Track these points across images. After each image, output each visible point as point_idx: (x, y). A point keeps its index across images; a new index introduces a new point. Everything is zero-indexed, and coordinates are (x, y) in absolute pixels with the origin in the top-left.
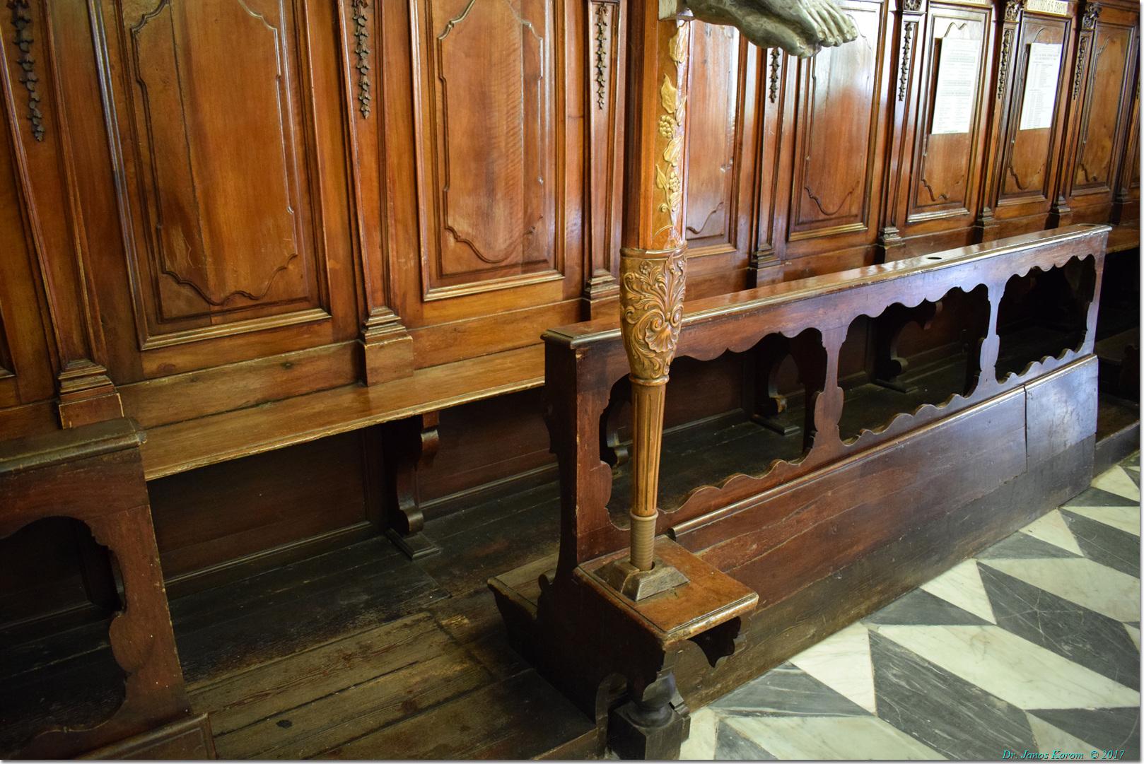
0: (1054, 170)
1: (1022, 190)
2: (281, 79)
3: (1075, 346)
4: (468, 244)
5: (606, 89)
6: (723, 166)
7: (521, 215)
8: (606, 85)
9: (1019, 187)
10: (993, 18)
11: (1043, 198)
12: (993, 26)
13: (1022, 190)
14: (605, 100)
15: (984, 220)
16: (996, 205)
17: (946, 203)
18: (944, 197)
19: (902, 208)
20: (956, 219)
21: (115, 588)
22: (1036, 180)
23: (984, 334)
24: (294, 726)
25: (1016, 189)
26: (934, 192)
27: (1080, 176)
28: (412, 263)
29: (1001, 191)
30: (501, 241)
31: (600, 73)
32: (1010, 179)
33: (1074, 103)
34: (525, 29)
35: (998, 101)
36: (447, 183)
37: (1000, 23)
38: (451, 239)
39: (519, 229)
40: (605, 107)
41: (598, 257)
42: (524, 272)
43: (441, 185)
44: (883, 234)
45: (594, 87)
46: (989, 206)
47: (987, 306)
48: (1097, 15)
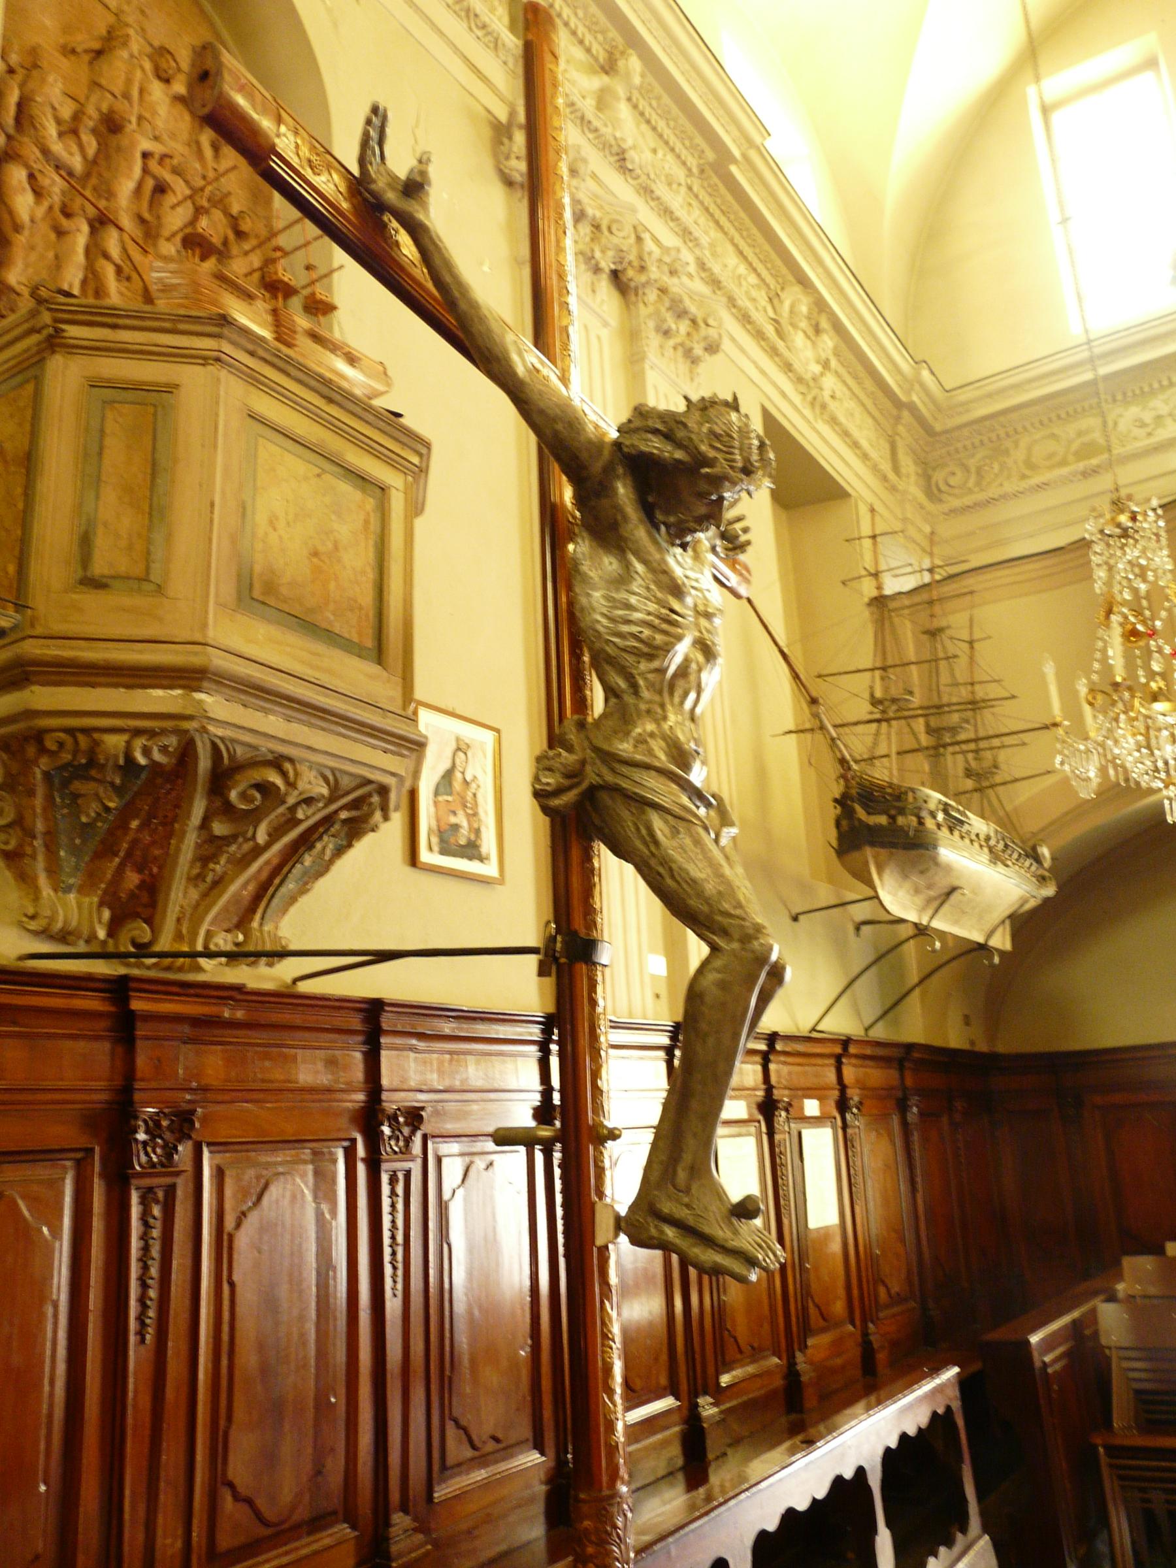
0: (855, 1292)
1: (828, 1322)
2: (56, 1306)
3: (964, 1530)
4: (249, 1502)
5: (400, 1272)
6: (522, 1349)
7: (310, 1450)
8: (400, 1266)
9: (824, 1319)
10: (764, 1129)
11: (851, 1328)
12: (765, 1138)
13: (828, 1322)
14: (400, 1286)
15: (799, 1367)
16: (806, 1347)
17: (756, 1353)
18: (753, 1348)
19: (711, 1370)
20: (768, 1373)
21: (562, 1125)
22: (839, 1307)
23: (874, 1530)
24: (672, 350)
25: (822, 1323)
26: (741, 1342)
27: (882, 1291)
28: (179, 1544)
29: (807, 1330)
30: (286, 1490)
31: (394, 1254)
32: (812, 1310)
33: (857, 1209)
34: (319, 1215)
35: (785, 1221)
36: (229, 1418)
37: (771, 1133)
38: (229, 1499)
39: (308, 1467)
40: (400, 1293)
41: (395, 1496)
42: (309, 1533)
43: (222, 1423)
44: (697, 1405)
45: (388, 1270)
46: (800, 1350)
47: (869, 1490)
48: (859, 1109)
